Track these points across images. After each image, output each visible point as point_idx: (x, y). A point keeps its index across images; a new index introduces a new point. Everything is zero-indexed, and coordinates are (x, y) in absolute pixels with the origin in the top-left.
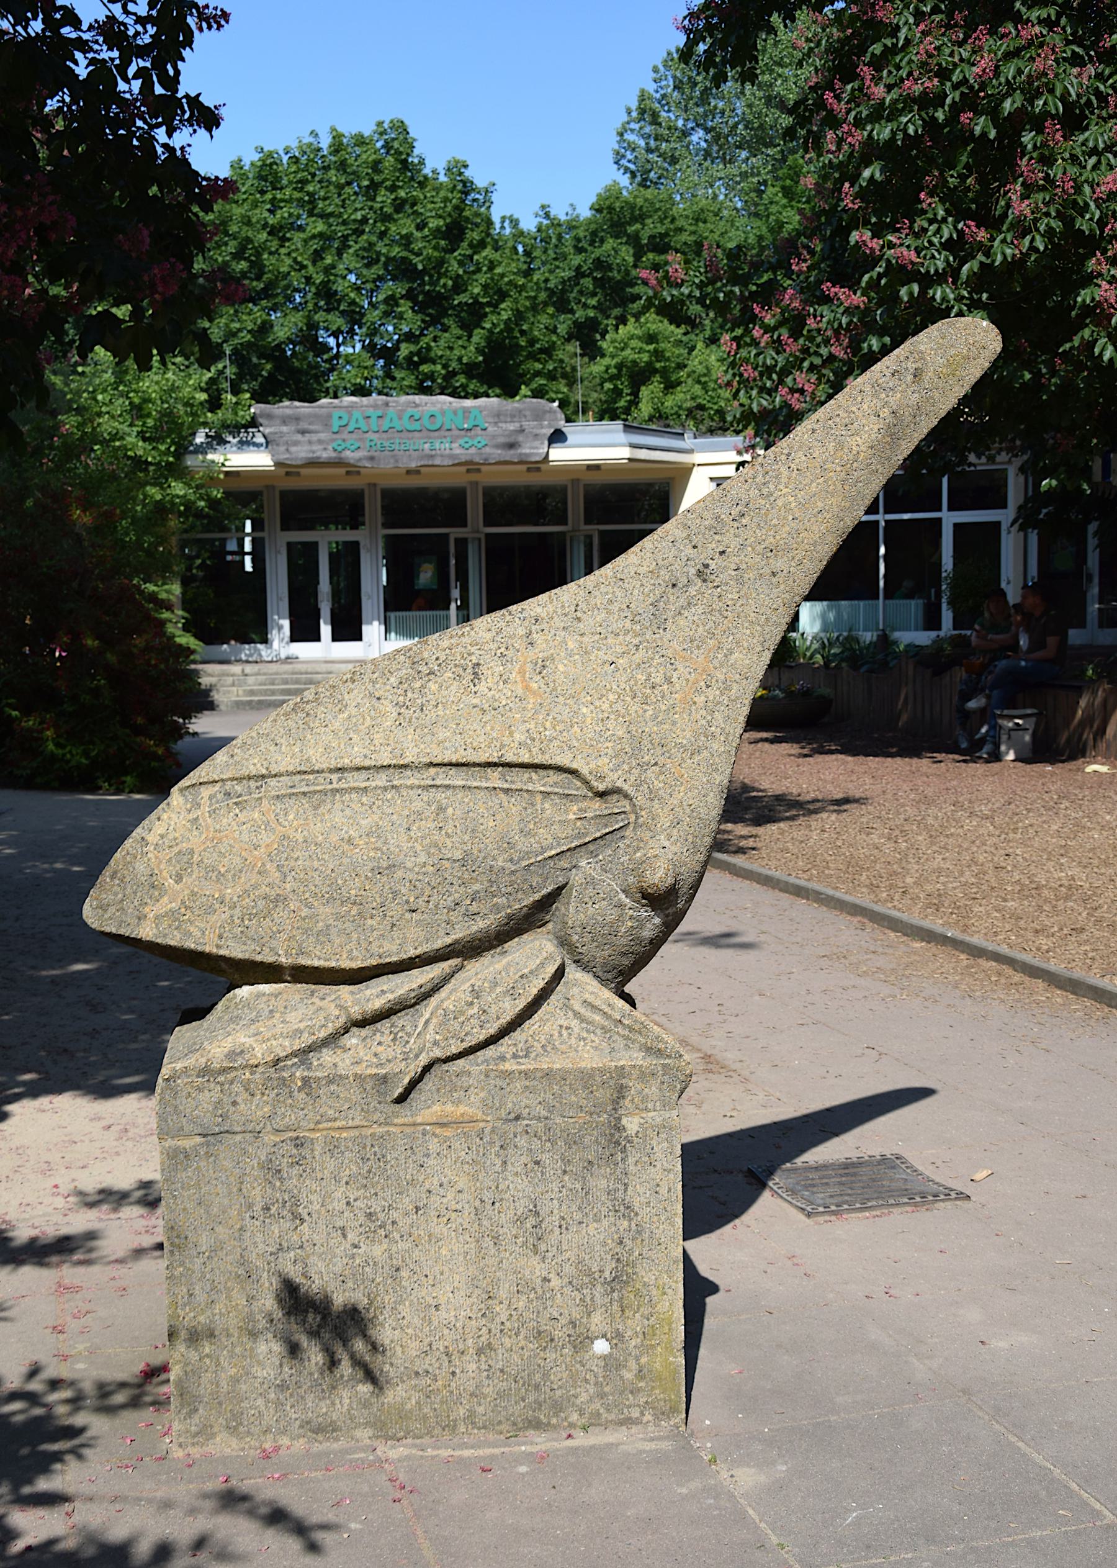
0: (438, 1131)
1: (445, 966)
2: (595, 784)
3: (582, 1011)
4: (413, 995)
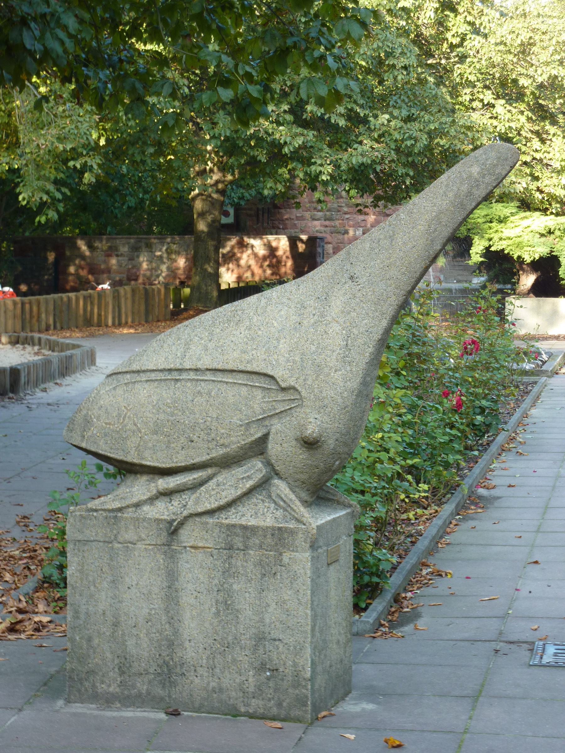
0: (193, 551)
1: (210, 471)
2: (281, 383)
3: (276, 500)
4: (190, 483)
